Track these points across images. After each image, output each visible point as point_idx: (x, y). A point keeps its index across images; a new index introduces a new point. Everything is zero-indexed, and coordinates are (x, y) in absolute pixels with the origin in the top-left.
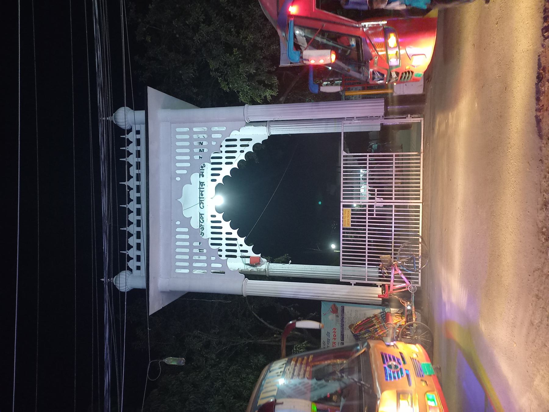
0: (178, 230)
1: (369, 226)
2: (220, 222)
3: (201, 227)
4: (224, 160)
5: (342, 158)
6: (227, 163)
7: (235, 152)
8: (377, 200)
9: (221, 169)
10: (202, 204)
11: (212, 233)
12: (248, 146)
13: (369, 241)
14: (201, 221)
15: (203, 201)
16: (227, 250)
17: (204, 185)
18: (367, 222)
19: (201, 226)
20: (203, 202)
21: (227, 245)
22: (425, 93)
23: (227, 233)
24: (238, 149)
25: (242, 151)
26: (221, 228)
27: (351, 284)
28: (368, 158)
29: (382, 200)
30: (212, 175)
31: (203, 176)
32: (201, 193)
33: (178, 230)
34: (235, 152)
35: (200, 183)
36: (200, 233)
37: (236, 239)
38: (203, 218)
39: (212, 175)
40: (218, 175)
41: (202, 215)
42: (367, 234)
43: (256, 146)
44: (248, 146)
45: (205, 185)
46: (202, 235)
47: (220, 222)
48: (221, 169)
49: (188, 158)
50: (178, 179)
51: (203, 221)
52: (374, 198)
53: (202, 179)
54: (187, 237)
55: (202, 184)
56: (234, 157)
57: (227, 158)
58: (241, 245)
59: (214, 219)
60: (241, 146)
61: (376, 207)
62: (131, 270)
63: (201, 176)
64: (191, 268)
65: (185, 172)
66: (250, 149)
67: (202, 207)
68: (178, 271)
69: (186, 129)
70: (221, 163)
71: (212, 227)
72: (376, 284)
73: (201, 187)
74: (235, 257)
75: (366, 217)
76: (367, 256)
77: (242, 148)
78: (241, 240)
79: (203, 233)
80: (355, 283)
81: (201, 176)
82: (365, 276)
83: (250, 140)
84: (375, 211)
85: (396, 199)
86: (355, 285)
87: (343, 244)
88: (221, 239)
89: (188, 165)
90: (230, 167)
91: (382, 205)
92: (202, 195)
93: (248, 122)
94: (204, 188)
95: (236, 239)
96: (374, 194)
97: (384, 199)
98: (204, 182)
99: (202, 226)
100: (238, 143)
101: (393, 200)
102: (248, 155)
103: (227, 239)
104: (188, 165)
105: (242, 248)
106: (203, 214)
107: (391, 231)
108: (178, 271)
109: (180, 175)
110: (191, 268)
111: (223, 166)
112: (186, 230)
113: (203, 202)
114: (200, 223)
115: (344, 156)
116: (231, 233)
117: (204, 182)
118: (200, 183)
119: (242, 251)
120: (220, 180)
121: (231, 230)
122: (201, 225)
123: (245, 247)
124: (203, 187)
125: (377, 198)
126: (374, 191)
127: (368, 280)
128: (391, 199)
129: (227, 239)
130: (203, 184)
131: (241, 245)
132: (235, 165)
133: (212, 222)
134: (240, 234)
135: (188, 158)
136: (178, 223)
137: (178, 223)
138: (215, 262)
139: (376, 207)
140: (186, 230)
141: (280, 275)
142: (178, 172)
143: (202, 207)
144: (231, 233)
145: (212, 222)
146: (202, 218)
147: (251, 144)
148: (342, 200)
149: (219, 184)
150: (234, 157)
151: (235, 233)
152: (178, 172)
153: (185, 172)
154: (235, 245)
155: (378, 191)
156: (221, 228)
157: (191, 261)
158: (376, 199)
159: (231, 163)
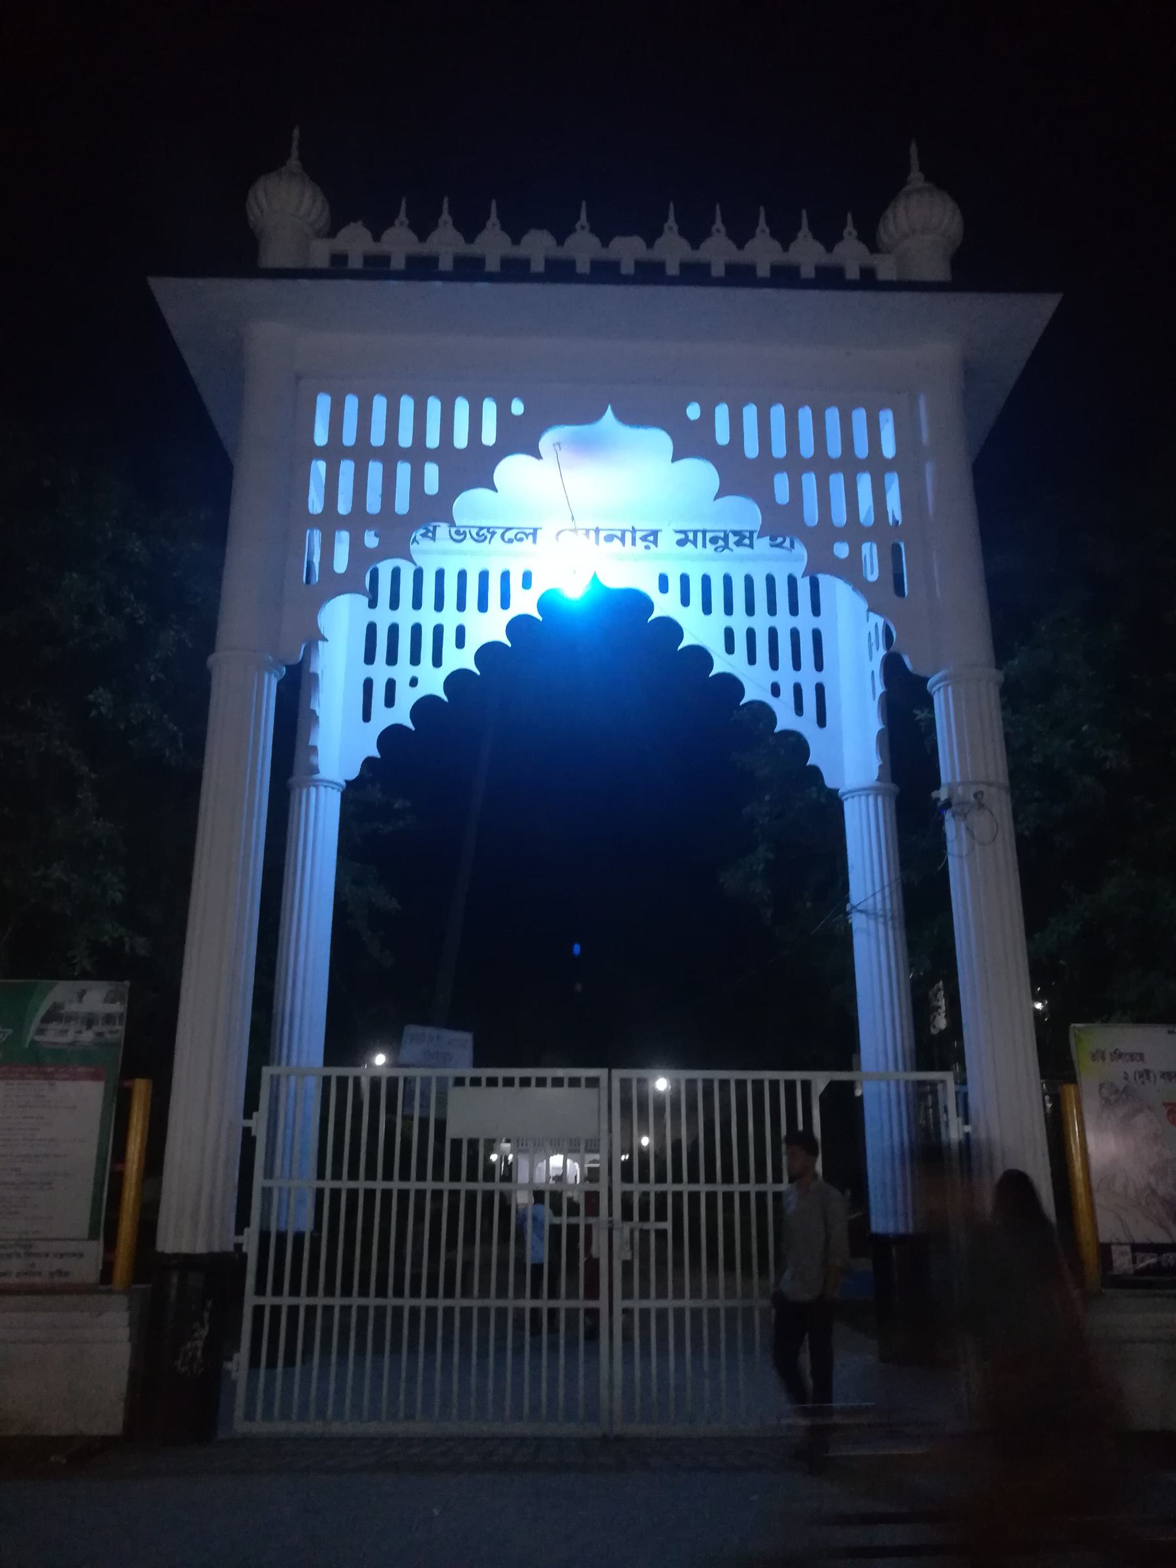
0: (490, 409)
1: (438, 1176)
2: (505, 603)
3: (484, 531)
4: (740, 622)
5: (797, 1076)
6: (729, 634)
7: (774, 664)
8: (623, 1232)
11: (462, 576)
12: (799, 709)
13: (371, 1175)
14: (510, 535)
16: (394, 630)
17: (647, 547)
19: (488, 531)
21: (417, 630)
22: (127, 1084)
23: (461, 632)
24: (786, 676)
25: (776, 690)
26: (483, 606)
27: (248, 1115)
29: (622, 1253)
30: (685, 580)
31: (681, 543)
32: (617, 537)
33: (490, 409)
34: (774, 664)
35: (655, 533)
36: (462, 531)
37: (437, 661)
38: (521, 540)
39: (685, 580)
40: (685, 601)
41: (531, 537)
43: (797, 744)
44: (799, 709)
45: (647, 551)
46: (455, 537)
47: (505, 603)
48: (707, 608)
49: (779, 449)
50: (693, 412)
51: (510, 541)
52: (627, 1215)
53: (668, 539)
54: (461, 440)
55: (651, 538)
56: (752, 660)
57: (751, 634)
58: (414, 682)
59: (516, 582)
60: (798, 689)
61: (589, 1228)
62: (332, 233)
64: (330, 521)
65: (722, 436)
66: (785, 720)
68: (324, 403)
69: (889, 449)
70: (729, 609)
71: (484, 577)
72: (257, 1110)
74: (369, 658)
77: (787, 693)
78: (433, 682)
79: (465, 536)
80: (253, 1133)
81: (682, 536)
83: (821, 721)
84: (573, 1220)
85: (627, 1312)
86: (247, 1131)
87: (426, 1081)
88: (439, 606)
89: (751, 449)
90: (715, 647)
91: (600, 1249)
92: (609, 538)
93: (933, 686)
94: (634, 543)
96: (644, 1216)
97: (627, 1266)
98: (657, 546)
100: (808, 677)
101: (619, 1304)
102: (763, 713)
103: (438, 631)
104: (751, 449)
106: (534, 541)
107: (485, 1294)
109: (708, 418)
110: (334, 453)
112: (489, 436)
114: (500, 532)
115: (806, 1085)
116: (460, 643)
117: (657, 546)
118: (655, 533)
119: (391, 685)
120: (665, 606)
121: (474, 643)
122: (493, 534)
123: (407, 699)
124: (638, 541)
125: (632, 1232)
126: (661, 1216)
127: (267, 1192)
128: (627, 1294)
129: (438, 631)
130: (650, 542)
131: (414, 682)
132: (721, 664)
133: (505, 577)
134: (456, 680)
135: (779, 449)
136: (517, 408)
137: (517, 408)
138: (356, 545)
139: (589, 1228)
140: (489, 436)
141: (293, 817)
142: (722, 413)
144: (460, 643)
145: (505, 577)
146: (518, 536)
147: (805, 725)
148: (618, 1074)
149: (649, 606)
150: (752, 660)
151: (462, 659)
152: (722, 413)
153: (722, 436)
154: (415, 659)
155: (661, 1234)
156: (483, 606)
157: (362, 453)
158: (627, 1227)
159: (730, 648)
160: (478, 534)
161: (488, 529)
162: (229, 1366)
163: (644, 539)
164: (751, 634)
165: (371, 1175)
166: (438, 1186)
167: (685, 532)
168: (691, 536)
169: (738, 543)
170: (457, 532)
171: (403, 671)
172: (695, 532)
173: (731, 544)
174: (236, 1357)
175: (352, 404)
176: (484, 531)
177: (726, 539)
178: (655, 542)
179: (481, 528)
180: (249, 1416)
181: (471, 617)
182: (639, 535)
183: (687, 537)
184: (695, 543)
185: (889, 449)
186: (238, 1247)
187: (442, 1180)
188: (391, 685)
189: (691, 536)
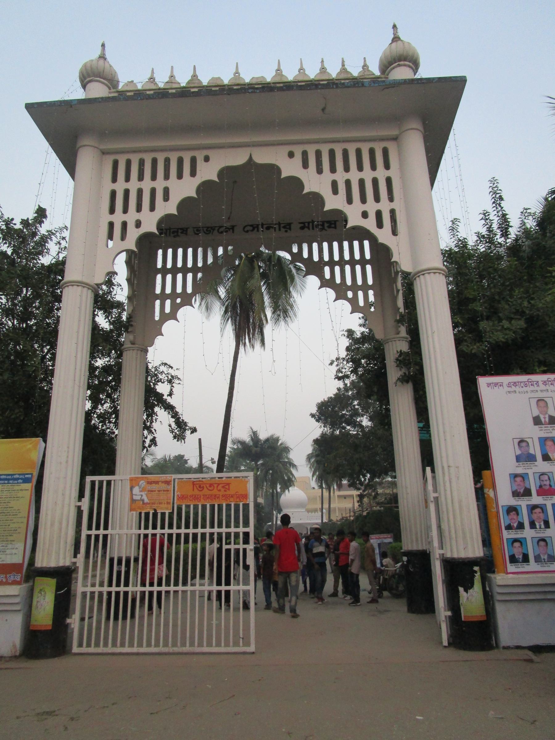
2: (193, 173)
6: (334, 185)
7: (363, 200)
9: (320, 171)
10: (251, 228)
13: (171, 527)
14: (221, 230)
15: (258, 231)
17: (286, 231)
18: (203, 531)
20: (256, 229)
23: (166, 192)
25: (365, 215)
26: (180, 176)
28: (94, 532)
31: (302, 228)
37: (152, 208)
41: (231, 230)
42: (179, 531)
46: (197, 232)
48: (320, 171)
56: (350, 201)
58: (138, 224)
63: (302, 225)
65: (305, 255)
67: (246, 229)
68: (160, 252)
73: (282, 225)
75: (169, 534)
76: (195, 531)
81: (302, 225)
82: (139, 535)
89: (316, 258)
90: (326, 192)
92: (268, 228)
95: (152, 208)
99: (212, 231)
100: (385, 206)
103: (153, 192)
104: (316, 258)
105: (131, 227)
106: (233, 232)
108: (160, 252)
111: (327, 176)
113: (256, 229)
114: (217, 228)
116: (166, 197)
118: (290, 224)
119: (124, 225)
122: (214, 230)
129: (153, 192)
130: (287, 228)
131: (138, 224)
142: (305, 247)
143: (246, 229)
152: (305, 247)
154: (139, 209)
159: (335, 191)
160: (207, 230)
161: (211, 228)
162: (68, 621)
163: (284, 227)
164: (348, 183)
165: (195, 526)
166: (237, 530)
167: (304, 223)
168: (307, 224)
169: (329, 227)
170: (198, 230)
171: (132, 216)
172: (309, 223)
173: (326, 228)
174: (74, 616)
175: (180, 251)
176: (210, 229)
177: (323, 225)
178: (290, 229)
179: (208, 228)
180: (80, 645)
181: (173, 183)
182: (282, 225)
183: (305, 225)
184: (309, 228)
185: (368, 256)
186: (75, 563)
187: (189, 528)
188: (124, 225)
189: (307, 224)
